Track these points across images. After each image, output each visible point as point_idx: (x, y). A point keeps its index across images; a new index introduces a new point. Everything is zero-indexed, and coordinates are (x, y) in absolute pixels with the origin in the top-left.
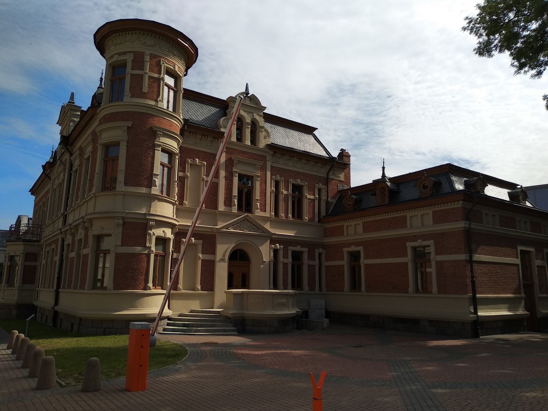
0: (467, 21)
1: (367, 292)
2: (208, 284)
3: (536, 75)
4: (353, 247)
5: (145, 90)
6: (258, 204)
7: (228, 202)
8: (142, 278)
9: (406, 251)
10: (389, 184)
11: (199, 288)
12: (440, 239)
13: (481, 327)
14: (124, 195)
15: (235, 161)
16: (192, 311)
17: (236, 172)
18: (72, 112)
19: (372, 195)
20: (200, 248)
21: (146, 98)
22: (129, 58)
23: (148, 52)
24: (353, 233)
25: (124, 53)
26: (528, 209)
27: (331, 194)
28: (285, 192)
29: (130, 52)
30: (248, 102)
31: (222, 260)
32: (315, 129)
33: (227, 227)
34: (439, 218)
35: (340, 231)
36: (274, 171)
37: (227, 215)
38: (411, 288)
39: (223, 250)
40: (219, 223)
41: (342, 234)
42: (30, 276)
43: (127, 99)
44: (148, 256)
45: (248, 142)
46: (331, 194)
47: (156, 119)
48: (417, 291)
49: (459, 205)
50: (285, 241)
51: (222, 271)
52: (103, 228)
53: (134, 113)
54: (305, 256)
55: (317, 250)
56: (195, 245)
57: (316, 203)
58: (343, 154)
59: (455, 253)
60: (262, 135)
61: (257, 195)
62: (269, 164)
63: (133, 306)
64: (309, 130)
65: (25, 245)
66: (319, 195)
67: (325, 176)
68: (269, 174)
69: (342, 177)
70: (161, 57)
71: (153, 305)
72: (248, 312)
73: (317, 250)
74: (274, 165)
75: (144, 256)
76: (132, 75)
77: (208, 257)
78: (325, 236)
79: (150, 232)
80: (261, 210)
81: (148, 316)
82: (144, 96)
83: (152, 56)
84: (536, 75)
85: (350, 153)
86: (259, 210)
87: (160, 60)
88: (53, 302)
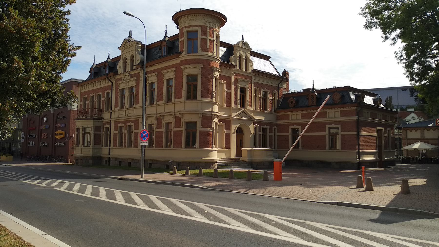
0: (362, 9)
2: (228, 146)
3: (393, 44)
4: (295, 126)
5: (208, 47)
7: (236, 103)
8: (211, 142)
9: (326, 129)
10: (316, 94)
12: (345, 126)
13: (360, 165)
14: (202, 102)
21: (208, 51)
22: (199, 29)
23: (208, 26)
26: (382, 109)
27: (280, 97)
30: (244, 47)
31: (234, 133)
32: (270, 57)
33: (236, 116)
34: (344, 114)
35: (287, 117)
36: (256, 84)
37: (236, 110)
38: (327, 147)
39: (234, 127)
41: (288, 119)
42: (97, 140)
43: (200, 52)
44: (213, 132)
45: (244, 70)
46: (280, 97)
48: (330, 149)
49: (354, 108)
50: (259, 123)
51: (233, 138)
54: (268, 131)
55: (273, 127)
56: (222, 125)
57: (273, 100)
58: (285, 73)
59: (351, 131)
60: (250, 64)
61: (248, 99)
62: (253, 81)
63: (208, 156)
64: (266, 58)
68: (253, 85)
71: (215, 156)
73: (273, 127)
77: (228, 132)
78: (277, 120)
82: (207, 50)
83: (211, 28)
84: (393, 44)
88: (108, 153)
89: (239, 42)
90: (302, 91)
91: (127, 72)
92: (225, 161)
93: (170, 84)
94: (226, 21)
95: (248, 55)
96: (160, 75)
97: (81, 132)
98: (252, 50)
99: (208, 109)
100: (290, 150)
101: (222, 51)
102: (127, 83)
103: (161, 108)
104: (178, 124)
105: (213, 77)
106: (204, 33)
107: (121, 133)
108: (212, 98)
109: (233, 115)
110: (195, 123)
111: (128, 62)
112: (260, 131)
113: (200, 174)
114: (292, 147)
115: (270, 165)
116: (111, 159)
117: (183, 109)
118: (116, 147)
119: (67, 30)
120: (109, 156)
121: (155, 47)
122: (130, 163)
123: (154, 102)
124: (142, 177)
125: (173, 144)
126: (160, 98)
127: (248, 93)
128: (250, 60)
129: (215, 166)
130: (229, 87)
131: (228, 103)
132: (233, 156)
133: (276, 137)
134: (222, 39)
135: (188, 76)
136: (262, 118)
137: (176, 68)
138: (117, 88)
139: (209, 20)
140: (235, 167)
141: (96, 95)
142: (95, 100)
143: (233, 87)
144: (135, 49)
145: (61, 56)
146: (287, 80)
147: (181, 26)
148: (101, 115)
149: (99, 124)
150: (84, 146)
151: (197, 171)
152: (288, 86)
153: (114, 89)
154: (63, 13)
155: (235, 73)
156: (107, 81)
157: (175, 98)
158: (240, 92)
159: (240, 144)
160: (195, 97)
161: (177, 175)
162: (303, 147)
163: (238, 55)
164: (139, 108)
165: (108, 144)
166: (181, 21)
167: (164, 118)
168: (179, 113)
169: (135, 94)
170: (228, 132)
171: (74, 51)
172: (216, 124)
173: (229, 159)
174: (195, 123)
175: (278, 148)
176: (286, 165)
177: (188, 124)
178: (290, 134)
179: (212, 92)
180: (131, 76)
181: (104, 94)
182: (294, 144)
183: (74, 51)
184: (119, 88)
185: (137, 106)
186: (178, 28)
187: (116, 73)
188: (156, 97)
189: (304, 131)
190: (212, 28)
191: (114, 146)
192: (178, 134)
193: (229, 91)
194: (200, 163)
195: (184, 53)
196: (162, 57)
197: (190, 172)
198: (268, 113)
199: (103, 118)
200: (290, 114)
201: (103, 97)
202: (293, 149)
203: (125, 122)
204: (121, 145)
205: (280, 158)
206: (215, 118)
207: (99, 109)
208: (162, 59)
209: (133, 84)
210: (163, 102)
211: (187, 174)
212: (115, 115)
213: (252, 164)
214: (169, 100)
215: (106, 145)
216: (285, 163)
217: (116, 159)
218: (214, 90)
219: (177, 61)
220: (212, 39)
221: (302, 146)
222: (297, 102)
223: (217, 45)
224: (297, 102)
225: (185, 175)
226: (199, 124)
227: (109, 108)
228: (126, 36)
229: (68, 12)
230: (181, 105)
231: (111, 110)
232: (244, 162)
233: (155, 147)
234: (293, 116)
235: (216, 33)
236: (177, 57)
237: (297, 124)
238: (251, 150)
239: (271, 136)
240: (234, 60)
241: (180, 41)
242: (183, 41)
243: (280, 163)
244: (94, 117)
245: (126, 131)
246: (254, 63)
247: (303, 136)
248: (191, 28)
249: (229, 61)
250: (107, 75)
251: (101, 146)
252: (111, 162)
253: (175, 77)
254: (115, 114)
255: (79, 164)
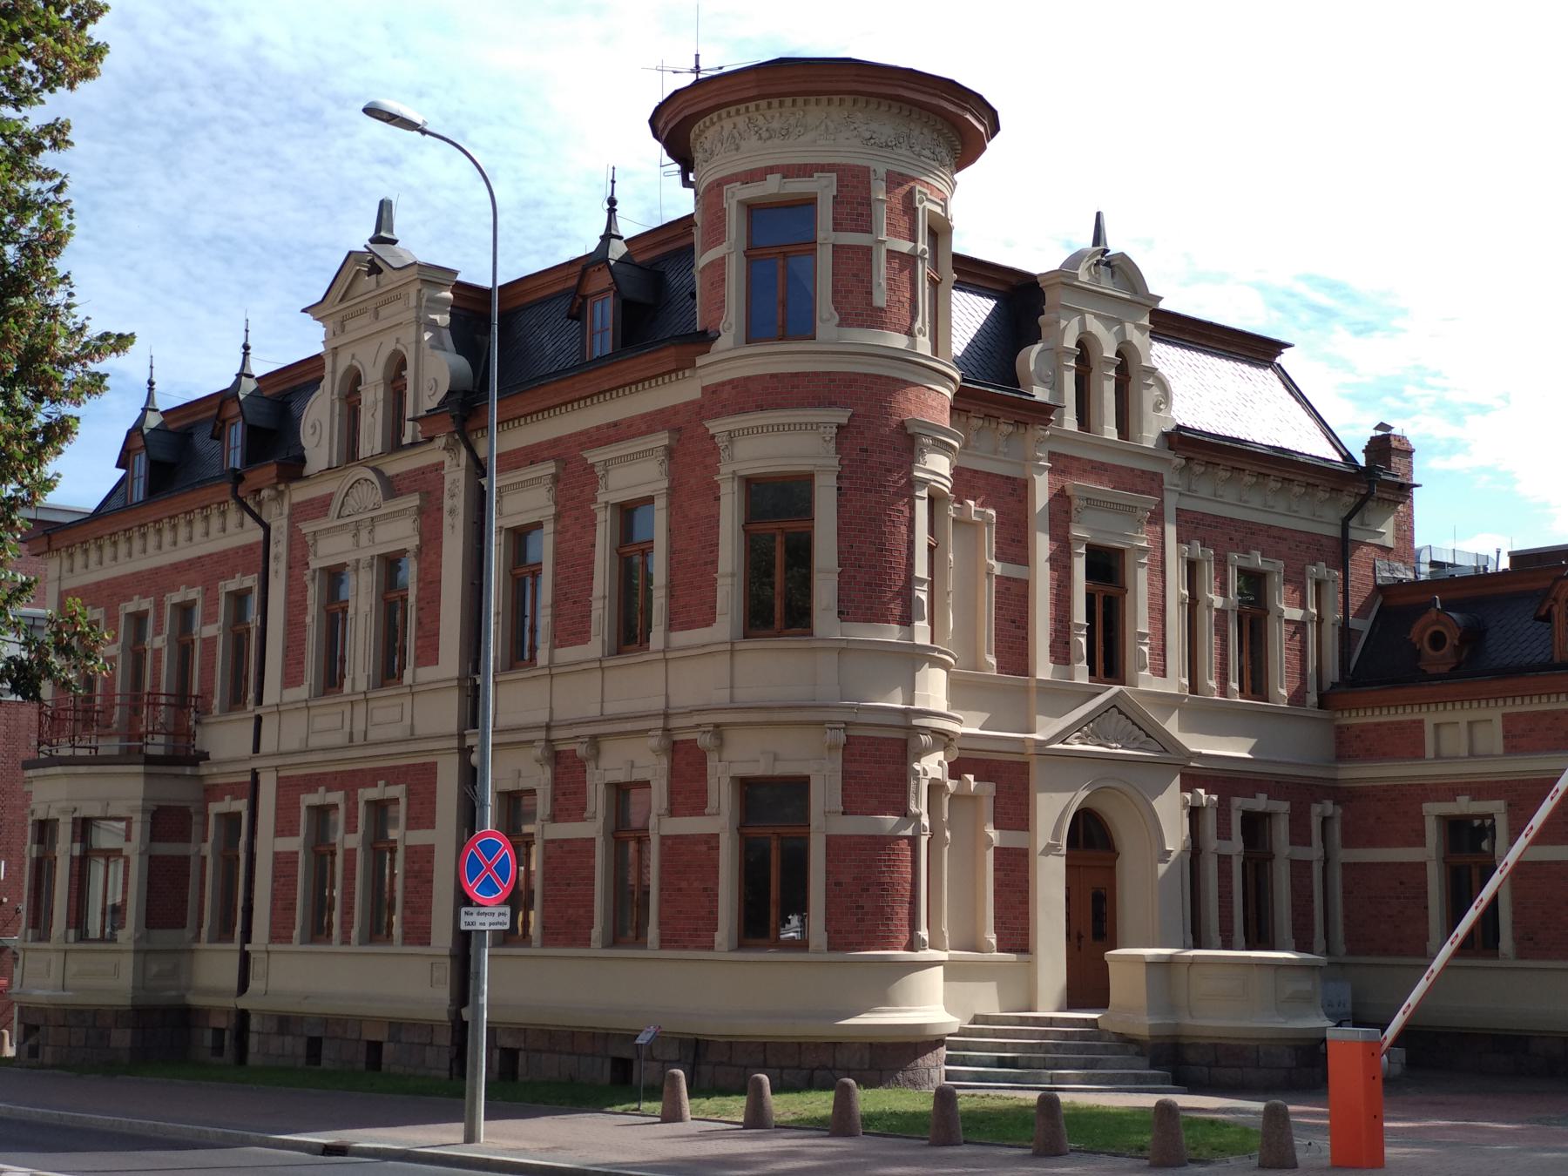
1: (1521, 955)
2: (1016, 933)
5: (880, 299)
6: (1146, 649)
7: (1061, 653)
8: (903, 912)
11: (994, 941)
14: (844, 650)
15: (1076, 502)
16: (976, 1019)
17: (1080, 540)
18: (427, 292)
19: (1537, 618)
20: (988, 807)
22: (824, 188)
24: (1464, 752)
25: (806, 171)
27: (1355, 602)
28: (1218, 602)
29: (823, 168)
30: (1107, 286)
31: (1050, 849)
32: (1276, 347)
33: (1062, 737)
35: (1409, 742)
36: (1191, 525)
37: (1059, 696)
39: (1052, 810)
40: (1040, 720)
41: (1417, 753)
44: (914, 842)
45: (1111, 432)
46: (1355, 602)
47: (911, 393)
51: (1050, 882)
52: (776, 759)
53: (851, 379)
55: (1316, 809)
56: (974, 798)
58: (1385, 447)
60: (1150, 396)
61: (1140, 619)
62: (1171, 502)
63: (884, 1000)
64: (1258, 350)
65: (147, 775)
66: (1318, 606)
67: (1335, 532)
68: (1171, 531)
69: (1387, 532)
70: (913, 179)
71: (930, 1002)
72: (1193, 1022)
73: (1316, 809)
74: (1188, 504)
75: (904, 844)
76: (837, 249)
77: (1015, 839)
79: (917, 766)
80: (1154, 672)
81: (929, 1032)
82: (874, 318)
83: (895, 180)
85: (1414, 442)
86: (1146, 673)
87: (911, 193)
89: (1075, 260)
90: (1505, 564)
91: (364, 463)
92: (995, 1034)
93: (639, 536)
94: (995, 128)
95: (1137, 338)
96: (573, 474)
97: (65, 848)
98: (1163, 305)
99: (885, 692)
100: (1437, 964)
101: (970, 314)
102: (357, 529)
103: (572, 688)
104: (688, 790)
105: (912, 484)
106: (855, 208)
107: (321, 852)
108: (907, 621)
109: (1045, 729)
110: (800, 785)
111: (373, 397)
112: (1224, 833)
113: (841, 1123)
114: (1447, 950)
115: (1302, 1067)
116: (254, 1024)
117: (722, 697)
118: (289, 939)
119: (55, 244)
120: (243, 1003)
121: (543, 301)
122: (375, 1048)
123: (533, 649)
124: (470, 1137)
125: (661, 924)
126: (572, 630)
127: (1141, 583)
128: (1152, 371)
129: (936, 1068)
130: (1014, 546)
131: (1015, 654)
132: (1049, 1006)
133: (1337, 876)
134: (964, 243)
135: (753, 486)
136: (1236, 749)
137: (676, 430)
138: (297, 563)
139: (884, 126)
140: (1063, 1079)
141: (159, 606)
142: (157, 642)
143: (1042, 545)
144: (411, 315)
145: (23, 402)
146: (1404, 490)
147: (706, 173)
148: (191, 735)
149: (175, 792)
150: (83, 936)
151: (820, 1103)
152: (1405, 531)
153: (278, 570)
154: (26, 136)
155: (1052, 456)
156: (233, 516)
157: (672, 626)
158: (1089, 576)
159: (1094, 924)
160: (799, 618)
161: (689, 1126)
162: (1528, 945)
163: (1070, 342)
164: (435, 688)
165: (233, 920)
166: (706, 137)
167: (598, 753)
168: (696, 720)
169: (412, 599)
170: (1015, 839)
171: (93, 367)
172: (935, 788)
173: (1023, 1021)
174: (800, 785)
175: (1351, 952)
176: (1412, 1063)
177: (750, 790)
178: (1429, 852)
179: (910, 580)
180: (392, 487)
181: (211, 601)
182: (1463, 928)
183: (93, 367)
184: (315, 564)
185: (426, 673)
186: (686, 183)
187: (294, 468)
188: (544, 620)
189: (1522, 842)
190: (907, 179)
191: (275, 937)
192: (689, 859)
193: (1014, 571)
194: (835, 1046)
195: (725, 341)
196: (586, 365)
197: (782, 1106)
198: (1278, 714)
199: (205, 756)
200: (1430, 717)
201: (209, 618)
202: (1458, 953)
203: (349, 781)
204: (319, 931)
205: (1366, 1016)
206: (928, 751)
207: (182, 698)
208: (580, 376)
209: (400, 533)
210: (594, 647)
211: (757, 1120)
212: (284, 735)
213: (1176, 1059)
214: (630, 634)
215: (223, 932)
216: (1401, 1053)
217: (284, 1023)
218: (921, 571)
219: (682, 391)
220: (905, 246)
221: (1518, 940)
222: (1474, 637)
223: (934, 284)
224: (1474, 637)
225: (746, 1125)
226: (824, 797)
227: (242, 687)
228: (359, 237)
229: (57, 134)
230: (705, 670)
231: (259, 700)
232: (1126, 1042)
233: (544, 945)
234: (1446, 733)
235: (926, 206)
236: (685, 365)
237: (1480, 790)
238: (1169, 962)
239: (1300, 869)
240: (1043, 374)
241: (702, 260)
242: (719, 264)
243: (1372, 1049)
244: (151, 750)
245: (354, 841)
246: (1175, 387)
247: (1520, 867)
248: (773, 186)
249: (1010, 377)
250: (237, 477)
251: (188, 934)
252: (253, 1041)
253: (673, 492)
254: (289, 729)
255: (47, 1055)
